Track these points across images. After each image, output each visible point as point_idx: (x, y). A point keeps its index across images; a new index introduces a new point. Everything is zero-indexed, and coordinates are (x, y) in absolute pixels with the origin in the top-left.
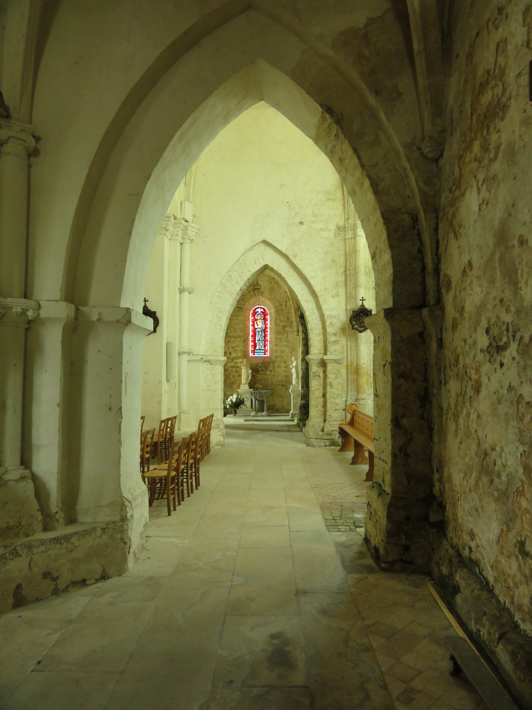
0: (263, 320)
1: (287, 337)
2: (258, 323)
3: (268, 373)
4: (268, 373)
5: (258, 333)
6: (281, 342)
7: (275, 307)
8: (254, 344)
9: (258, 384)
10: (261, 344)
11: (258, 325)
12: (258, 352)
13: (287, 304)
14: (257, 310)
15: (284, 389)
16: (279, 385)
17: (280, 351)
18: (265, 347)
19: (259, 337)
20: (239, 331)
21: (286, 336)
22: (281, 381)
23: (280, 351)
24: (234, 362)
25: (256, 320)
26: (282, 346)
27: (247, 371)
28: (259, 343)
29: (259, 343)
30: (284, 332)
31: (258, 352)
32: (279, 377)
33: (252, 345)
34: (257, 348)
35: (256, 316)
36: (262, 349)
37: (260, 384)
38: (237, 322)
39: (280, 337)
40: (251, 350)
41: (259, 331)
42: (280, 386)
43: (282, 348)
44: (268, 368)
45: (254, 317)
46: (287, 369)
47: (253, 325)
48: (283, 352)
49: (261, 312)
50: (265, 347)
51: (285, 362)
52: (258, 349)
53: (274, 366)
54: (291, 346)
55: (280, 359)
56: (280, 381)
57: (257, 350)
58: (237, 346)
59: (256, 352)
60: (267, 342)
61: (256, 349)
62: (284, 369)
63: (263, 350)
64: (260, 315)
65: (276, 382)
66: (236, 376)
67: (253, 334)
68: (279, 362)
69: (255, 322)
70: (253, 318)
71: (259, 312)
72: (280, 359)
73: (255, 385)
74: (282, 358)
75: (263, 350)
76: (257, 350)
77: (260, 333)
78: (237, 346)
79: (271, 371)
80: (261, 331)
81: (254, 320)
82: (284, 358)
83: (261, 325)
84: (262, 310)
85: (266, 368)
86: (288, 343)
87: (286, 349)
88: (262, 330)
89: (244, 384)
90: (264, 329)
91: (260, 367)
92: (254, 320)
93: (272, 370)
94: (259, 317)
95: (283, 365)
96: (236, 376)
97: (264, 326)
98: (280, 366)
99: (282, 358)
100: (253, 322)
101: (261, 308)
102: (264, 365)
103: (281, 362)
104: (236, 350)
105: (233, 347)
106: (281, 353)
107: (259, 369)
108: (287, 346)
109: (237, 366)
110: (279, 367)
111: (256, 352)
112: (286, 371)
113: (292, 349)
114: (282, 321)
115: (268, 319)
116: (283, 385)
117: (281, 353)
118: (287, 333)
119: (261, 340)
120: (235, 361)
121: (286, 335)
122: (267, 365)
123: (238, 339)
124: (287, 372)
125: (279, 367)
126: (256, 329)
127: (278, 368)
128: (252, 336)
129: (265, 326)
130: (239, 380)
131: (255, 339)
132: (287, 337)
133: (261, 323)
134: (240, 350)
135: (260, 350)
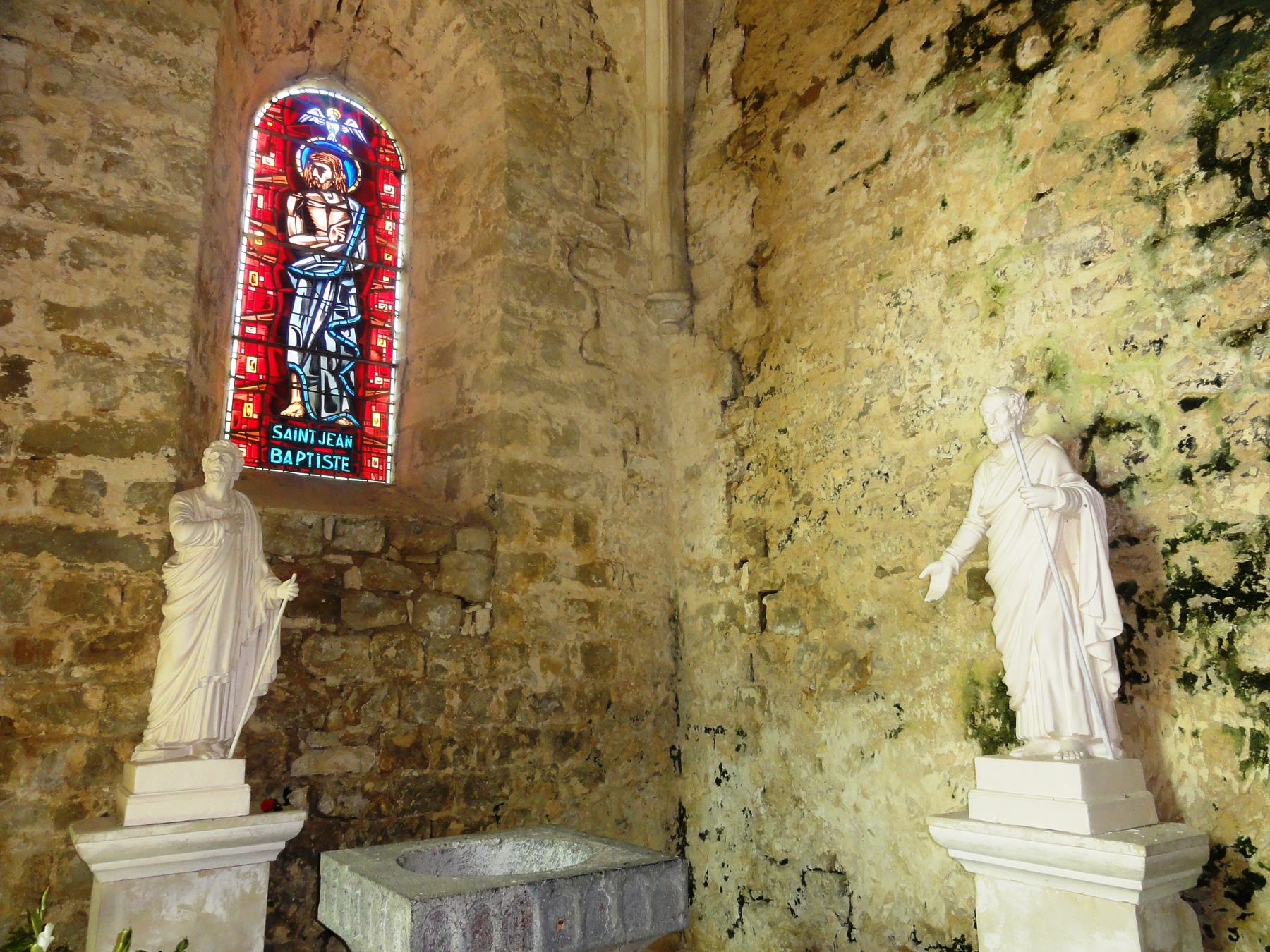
0: (353, 204)
1: (597, 325)
2: (318, 215)
3: (438, 618)
4: (438, 618)
5: (312, 290)
6: (553, 358)
7: (512, 80)
8: (262, 367)
9: (330, 739)
10: (333, 383)
11: (310, 228)
12: (295, 446)
13: (595, 93)
14: (313, 115)
15: (577, 772)
16: (533, 735)
17: (546, 431)
18: (360, 408)
19: (318, 324)
20: (156, 169)
21: (587, 315)
22: (549, 696)
23: (546, 431)
24: (48, 487)
25: (300, 185)
26: (560, 393)
27: (238, 599)
28: (316, 370)
29: (316, 370)
30: (577, 287)
31: (295, 446)
32: (535, 662)
33: (251, 379)
34: (294, 409)
35: (300, 156)
36: (332, 427)
37: (349, 742)
38: (138, 70)
39: (542, 311)
40: (237, 420)
41: (323, 273)
42: (544, 753)
43: (560, 413)
44: (437, 570)
45: (287, 161)
46: (593, 594)
47: (274, 217)
48: (566, 440)
49: (350, 140)
50: (360, 408)
51: (582, 531)
52: (304, 422)
53: (491, 554)
54: (626, 402)
55: (542, 501)
56: (539, 701)
57: (289, 423)
58: (114, 312)
59: (286, 445)
60: (385, 374)
61: (288, 412)
62: (578, 590)
63: (344, 431)
64: (331, 158)
65: (512, 713)
66: (65, 653)
67: (261, 289)
68: (536, 523)
69: (291, 202)
70: (270, 161)
71: (332, 137)
72: (542, 501)
73: (294, 750)
74: (556, 491)
75: (344, 431)
76: (289, 423)
77: (328, 294)
78: (114, 312)
79: (466, 604)
80: (336, 281)
81: (284, 180)
82: (570, 492)
83: (339, 232)
84: (352, 125)
85: (418, 571)
86: (604, 373)
87: (593, 423)
88: (346, 275)
89: (176, 753)
90: (359, 267)
91: (362, 557)
92: (284, 180)
93: (479, 593)
94: (328, 174)
95: (562, 548)
96: (65, 653)
97: (362, 246)
98: (541, 557)
99: (556, 491)
100: (276, 196)
101: (347, 111)
102: (399, 542)
103: (549, 530)
104: (103, 352)
105: (57, 315)
106: (553, 452)
107: (354, 579)
108: (598, 402)
109: (84, 522)
110: (535, 566)
111: (286, 445)
112: (593, 607)
113: (628, 426)
114: (557, 199)
115: (396, 201)
116: (566, 742)
117: (553, 452)
118: (596, 301)
119: (331, 345)
120: (69, 465)
121: (590, 309)
122: (434, 544)
123: (138, 246)
124: (594, 619)
125: (535, 566)
126: (298, 252)
127: (532, 575)
128: (255, 302)
129: (375, 251)
130: (94, 699)
131: (279, 329)
132: (597, 325)
133: (337, 216)
134: (153, 360)
135: (320, 427)
